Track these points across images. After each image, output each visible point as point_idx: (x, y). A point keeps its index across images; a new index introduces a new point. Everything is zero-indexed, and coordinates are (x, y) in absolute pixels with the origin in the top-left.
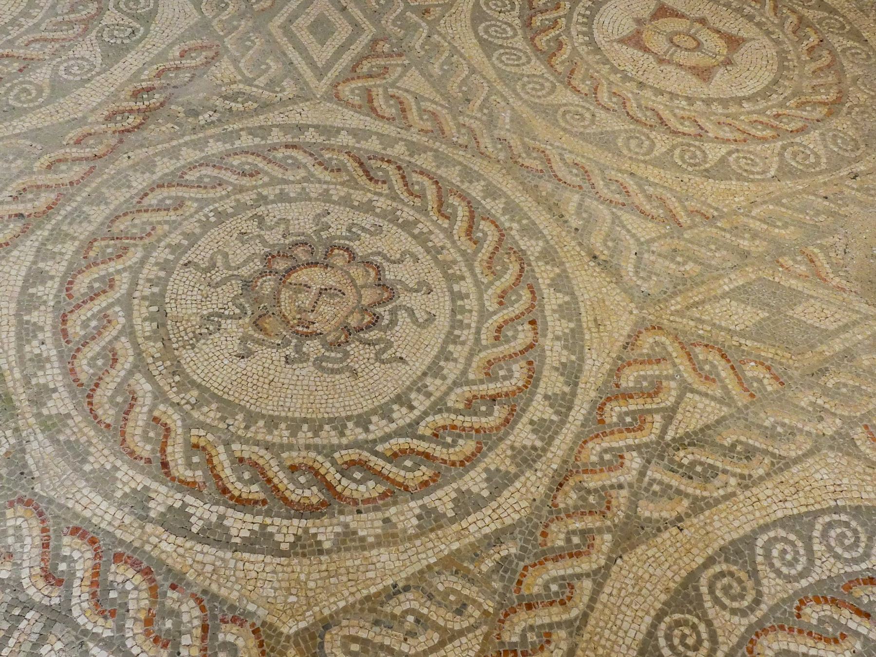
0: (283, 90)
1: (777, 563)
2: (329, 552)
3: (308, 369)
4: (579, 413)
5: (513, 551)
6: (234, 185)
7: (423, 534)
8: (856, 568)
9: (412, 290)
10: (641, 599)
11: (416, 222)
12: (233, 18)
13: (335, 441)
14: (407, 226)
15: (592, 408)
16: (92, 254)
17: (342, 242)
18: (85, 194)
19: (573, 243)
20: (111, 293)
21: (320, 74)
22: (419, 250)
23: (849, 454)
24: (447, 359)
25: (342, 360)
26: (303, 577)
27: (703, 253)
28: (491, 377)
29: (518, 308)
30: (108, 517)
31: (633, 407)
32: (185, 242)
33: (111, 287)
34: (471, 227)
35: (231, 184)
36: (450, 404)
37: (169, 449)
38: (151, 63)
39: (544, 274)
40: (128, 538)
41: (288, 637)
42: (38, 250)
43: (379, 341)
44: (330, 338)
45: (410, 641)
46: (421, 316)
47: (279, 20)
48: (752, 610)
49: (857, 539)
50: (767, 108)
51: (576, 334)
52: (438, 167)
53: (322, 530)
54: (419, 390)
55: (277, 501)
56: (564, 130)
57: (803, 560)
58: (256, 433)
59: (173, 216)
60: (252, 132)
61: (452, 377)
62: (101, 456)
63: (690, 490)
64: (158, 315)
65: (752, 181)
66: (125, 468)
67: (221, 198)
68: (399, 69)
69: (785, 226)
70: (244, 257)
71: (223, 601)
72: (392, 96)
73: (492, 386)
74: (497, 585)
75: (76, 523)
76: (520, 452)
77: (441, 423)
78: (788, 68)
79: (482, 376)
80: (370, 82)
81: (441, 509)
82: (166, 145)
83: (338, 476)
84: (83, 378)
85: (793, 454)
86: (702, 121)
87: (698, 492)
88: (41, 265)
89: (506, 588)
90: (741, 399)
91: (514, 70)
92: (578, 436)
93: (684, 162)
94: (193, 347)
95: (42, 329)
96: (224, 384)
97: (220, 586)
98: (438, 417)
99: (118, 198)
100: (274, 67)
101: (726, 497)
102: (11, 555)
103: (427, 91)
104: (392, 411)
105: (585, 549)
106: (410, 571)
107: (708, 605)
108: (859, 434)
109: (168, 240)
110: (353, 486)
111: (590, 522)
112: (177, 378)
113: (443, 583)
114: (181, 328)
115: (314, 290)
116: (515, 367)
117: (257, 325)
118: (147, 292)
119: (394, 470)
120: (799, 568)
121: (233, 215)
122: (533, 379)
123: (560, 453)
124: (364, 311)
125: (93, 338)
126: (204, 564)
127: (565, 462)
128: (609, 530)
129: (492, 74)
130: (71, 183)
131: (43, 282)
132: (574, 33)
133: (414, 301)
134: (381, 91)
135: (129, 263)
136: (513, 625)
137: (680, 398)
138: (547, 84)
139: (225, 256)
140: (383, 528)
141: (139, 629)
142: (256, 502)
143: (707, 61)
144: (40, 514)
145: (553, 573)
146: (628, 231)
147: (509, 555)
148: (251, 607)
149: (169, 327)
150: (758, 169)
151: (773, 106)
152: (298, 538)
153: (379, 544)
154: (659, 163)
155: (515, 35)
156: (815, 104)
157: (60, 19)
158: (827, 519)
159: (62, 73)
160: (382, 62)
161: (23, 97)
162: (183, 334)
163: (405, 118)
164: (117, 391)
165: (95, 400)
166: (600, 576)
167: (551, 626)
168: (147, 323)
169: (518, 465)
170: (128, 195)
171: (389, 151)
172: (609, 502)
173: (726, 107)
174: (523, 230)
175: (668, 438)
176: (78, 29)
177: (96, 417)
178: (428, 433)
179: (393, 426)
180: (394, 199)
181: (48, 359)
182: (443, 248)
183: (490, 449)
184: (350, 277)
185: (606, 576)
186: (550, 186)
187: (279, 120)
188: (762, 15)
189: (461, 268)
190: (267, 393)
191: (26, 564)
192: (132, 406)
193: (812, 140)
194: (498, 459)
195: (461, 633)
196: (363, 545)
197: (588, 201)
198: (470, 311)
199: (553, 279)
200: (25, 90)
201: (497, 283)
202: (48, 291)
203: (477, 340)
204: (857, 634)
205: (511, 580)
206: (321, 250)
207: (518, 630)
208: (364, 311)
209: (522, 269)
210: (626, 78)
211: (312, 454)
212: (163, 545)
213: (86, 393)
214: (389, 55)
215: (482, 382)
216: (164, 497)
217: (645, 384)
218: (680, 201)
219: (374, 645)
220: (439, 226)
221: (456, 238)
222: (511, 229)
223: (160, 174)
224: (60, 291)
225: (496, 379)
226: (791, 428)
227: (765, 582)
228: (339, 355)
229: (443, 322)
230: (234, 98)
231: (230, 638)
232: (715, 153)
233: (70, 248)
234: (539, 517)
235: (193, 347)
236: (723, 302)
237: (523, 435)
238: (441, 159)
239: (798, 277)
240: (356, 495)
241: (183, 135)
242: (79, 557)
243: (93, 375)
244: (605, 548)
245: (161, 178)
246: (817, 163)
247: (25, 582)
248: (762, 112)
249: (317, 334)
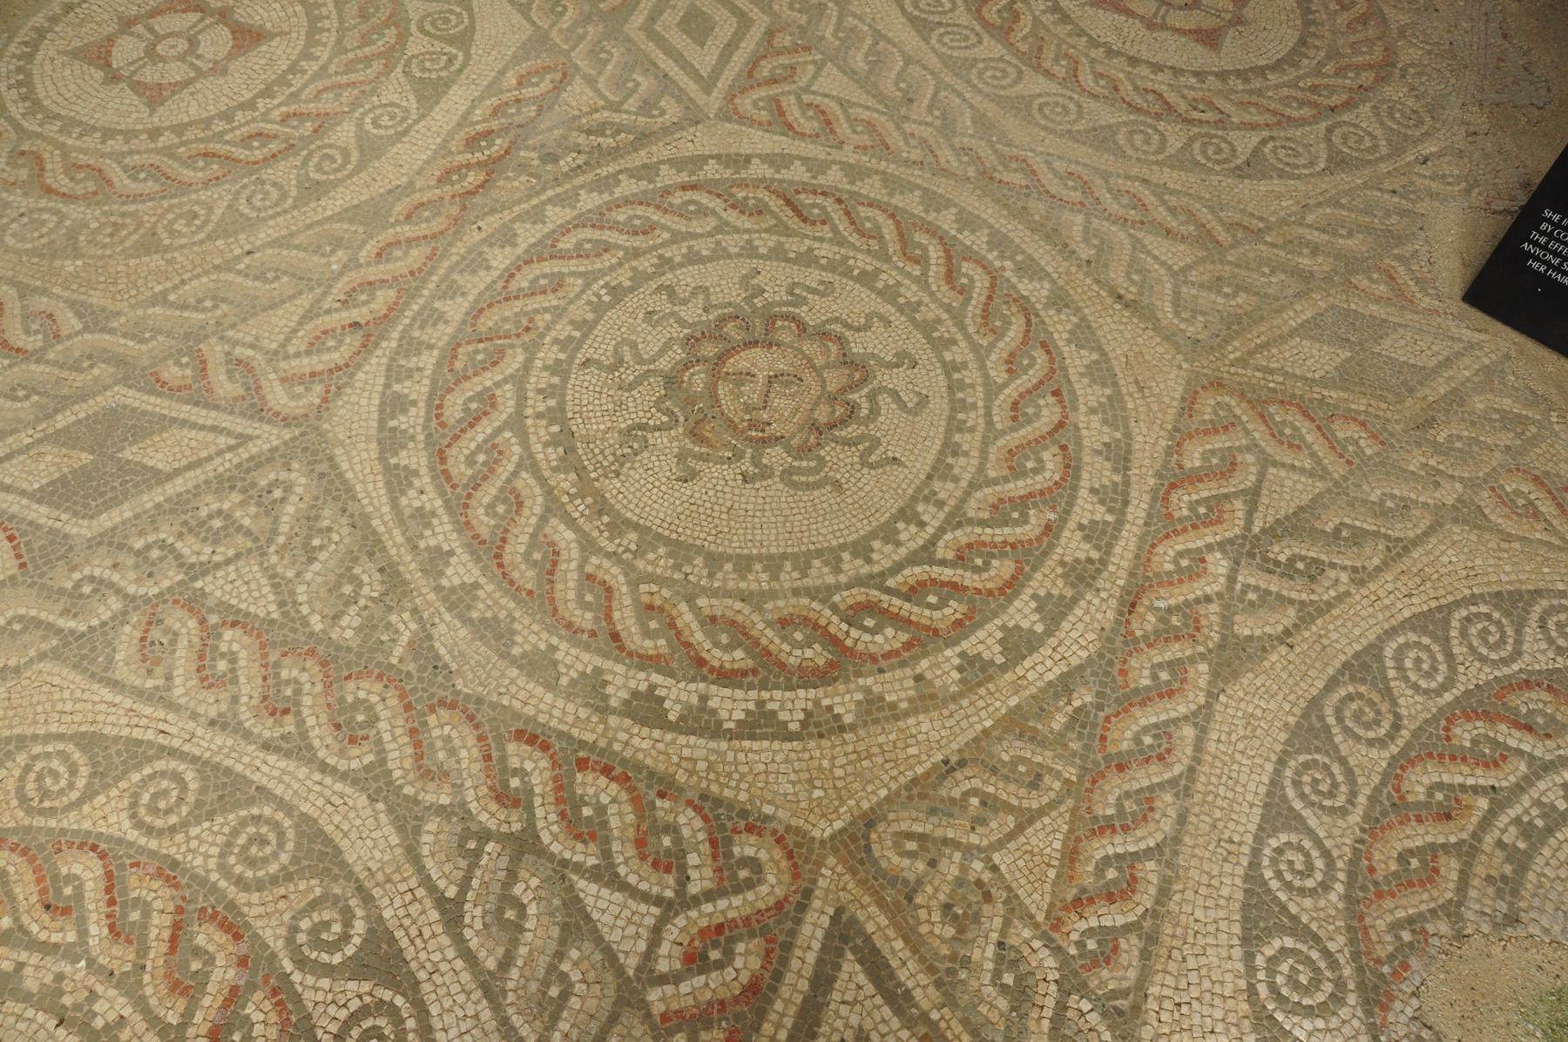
0: (663, 112)
1: (1413, 677)
3: (776, 484)
4: (1137, 511)
5: (1088, 699)
7: (970, 690)
8: (1506, 671)
9: (890, 366)
10: (1256, 743)
11: (878, 271)
12: (576, 24)
13: (830, 579)
14: (866, 278)
15: (1154, 500)
16: (458, 365)
18: (431, 286)
19: (1088, 281)
20: (495, 415)
21: (707, 85)
22: (887, 309)
23: (1479, 527)
24: (955, 454)
25: (817, 470)
26: (826, 763)
28: (1017, 473)
30: (556, 713)
31: (1205, 494)
32: (577, 334)
33: (493, 406)
35: (618, 247)
36: (971, 514)
37: (616, 615)
38: (481, 98)
39: (1059, 326)
40: (589, 737)
41: (823, 842)
42: (389, 369)
44: (796, 442)
45: (979, 829)
46: (910, 399)
47: (638, 19)
48: (1392, 739)
49: (1503, 633)
50: (1300, 78)
52: (891, 195)
53: (838, 699)
54: (926, 500)
55: (767, 669)
56: (1045, 128)
57: (1443, 668)
58: (725, 580)
59: (552, 300)
60: (634, 174)
62: (531, 635)
63: (1294, 595)
65: (1299, 177)
66: (564, 646)
67: (612, 268)
68: (811, 68)
69: (1350, 234)
70: (659, 344)
72: (810, 105)
73: (1020, 483)
74: (1075, 746)
75: (520, 725)
77: (964, 540)
78: (1314, 23)
79: (1006, 472)
80: (776, 90)
81: (986, 655)
82: (525, 206)
83: (844, 626)
84: (484, 532)
85: (1411, 534)
87: (1304, 596)
88: (396, 387)
89: (1086, 747)
90: (1338, 470)
93: (1208, 158)
95: (416, 473)
97: (722, 786)
98: (958, 533)
101: (1340, 598)
102: (447, 774)
103: (856, 95)
104: (897, 532)
105: (1176, 685)
106: (962, 740)
107: (1338, 739)
108: (1485, 498)
109: (553, 334)
110: (867, 637)
111: (1175, 651)
112: (606, 519)
115: (761, 377)
116: (1046, 456)
117: (695, 435)
118: (541, 407)
119: (916, 609)
120: (1440, 679)
121: (632, 289)
122: (1072, 469)
123: (1125, 564)
124: (832, 399)
125: (485, 478)
127: (1132, 574)
128: (1203, 657)
129: (936, 64)
130: (412, 273)
131: (404, 411)
133: (894, 379)
134: (792, 99)
135: (509, 371)
136: (1104, 793)
137: (1262, 475)
138: (1010, 70)
139: (633, 345)
140: (916, 689)
141: (631, 851)
142: (744, 673)
143: (1209, 23)
144: (471, 718)
145: (1144, 722)
146: (1156, 258)
148: (768, 810)
151: (1306, 76)
152: (808, 714)
153: (914, 711)
156: (1360, 68)
157: (351, 55)
158: (1464, 613)
159: (369, 127)
160: (784, 60)
161: (326, 166)
163: (833, 132)
165: (507, 559)
166: (1202, 718)
167: (1151, 788)
169: (1073, 585)
170: (489, 280)
171: (821, 180)
172: (1197, 621)
173: (1247, 81)
174: (1019, 269)
175: (1256, 529)
176: (377, 66)
177: (512, 583)
178: (950, 555)
179: (903, 551)
182: (919, 303)
183: (1034, 569)
185: (1209, 717)
186: (1042, 207)
187: (666, 154)
189: (948, 328)
191: (468, 784)
192: (555, 563)
195: (1041, 812)
197: (1096, 223)
198: (972, 386)
199: (1071, 332)
201: (1001, 344)
202: (412, 420)
203: (990, 424)
204: (1519, 752)
205: (1091, 736)
207: (1112, 799)
208: (832, 399)
210: (1110, 53)
211: (805, 601)
212: (636, 741)
213: (490, 551)
214: (794, 50)
215: (1006, 480)
216: (622, 682)
217: (1215, 461)
218: (1212, 210)
219: (934, 840)
220: (909, 275)
222: (1003, 268)
223: (524, 246)
224: (428, 420)
225: (1023, 474)
226: (1402, 499)
227: (1402, 701)
229: (939, 404)
230: (600, 130)
231: (750, 852)
232: (1245, 143)
233: (428, 360)
234: (1113, 651)
236: (1293, 343)
237: (1072, 546)
239: (1378, 300)
241: (544, 190)
242: (536, 770)
243: (497, 526)
244: (1202, 683)
245: (527, 251)
246: (1375, 147)
248: (1293, 84)
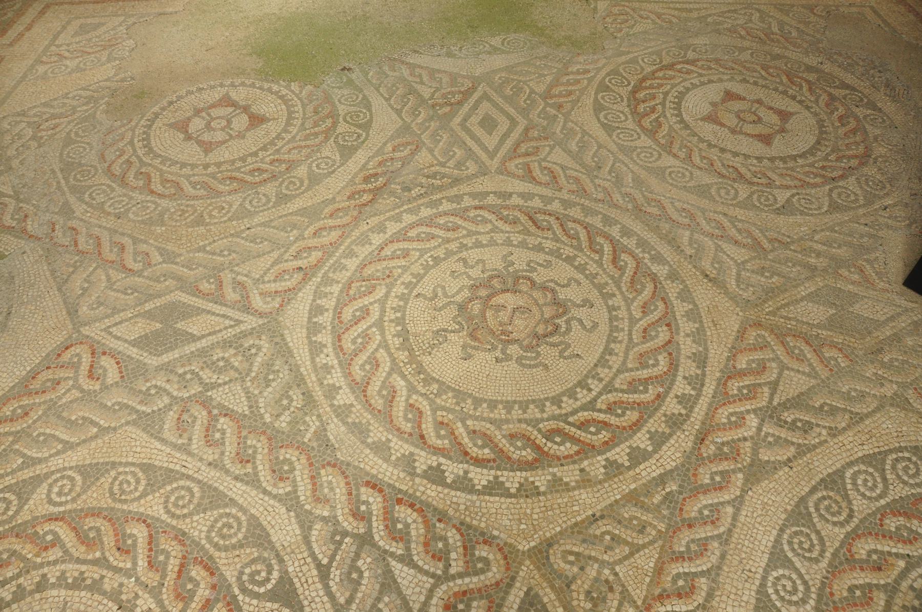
0: (467, 169)
1: (862, 489)
2: (544, 494)
3: (513, 364)
4: (709, 389)
5: (674, 488)
7: (610, 479)
9: (579, 306)
10: (768, 519)
11: (576, 256)
12: (425, 120)
13: (539, 416)
14: (569, 260)
15: (718, 384)
16: (351, 292)
21: (492, 155)
22: (580, 277)
24: (610, 354)
27: (785, 269)
28: (644, 366)
29: (656, 315)
30: (388, 474)
31: (747, 383)
33: (368, 314)
34: (614, 258)
36: (617, 386)
37: (424, 426)
38: (373, 157)
39: (672, 290)
40: (404, 488)
41: (523, 552)
42: (315, 292)
43: (561, 343)
44: (525, 343)
45: (609, 553)
46: (588, 324)
47: (457, 120)
48: (848, 522)
51: (701, 331)
52: (586, 217)
54: (593, 377)
55: (501, 460)
57: (880, 486)
58: (482, 412)
59: (403, 262)
60: (449, 199)
61: (616, 366)
62: (378, 433)
63: (795, 440)
66: (395, 440)
67: (435, 247)
69: (839, 247)
71: (476, 530)
73: (645, 371)
75: (368, 479)
76: (671, 418)
77: (612, 400)
79: (637, 365)
80: (528, 159)
83: (544, 440)
85: (865, 411)
86: (770, 174)
88: (319, 302)
90: (824, 373)
91: (629, 144)
92: (710, 405)
95: (325, 346)
97: (472, 518)
98: (609, 395)
99: (363, 252)
100: (459, 153)
101: (821, 443)
102: (328, 501)
103: (570, 163)
106: (603, 504)
107: (816, 520)
108: (910, 394)
110: (556, 447)
111: (725, 466)
112: (422, 376)
113: (628, 512)
115: (510, 308)
116: (660, 358)
117: (472, 336)
118: (393, 317)
120: (878, 491)
121: (444, 259)
122: (674, 366)
123: (699, 418)
124: (547, 322)
125: (361, 351)
126: (459, 505)
127: (703, 423)
128: (740, 470)
129: (614, 148)
132: (668, 115)
133: (582, 313)
134: (536, 164)
136: (679, 539)
137: (780, 374)
139: (443, 288)
142: (489, 461)
143: (766, 131)
144: (343, 473)
145: (704, 502)
147: (672, 491)
148: (496, 533)
150: (814, 206)
152: (521, 485)
153: (579, 487)
154: (743, 205)
155: (627, 119)
156: (850, 158)
158: (894, 456)
159: (315, 168)
164: (383, 387)
165: (369, 393)
166: (738, 503)
167: (706, 538)
169: (670, 427)
171: (549, 207)
173: (785, 162)
175: (775, 403)
176: (321, 138)
177: (370, 405)
178: (604, 407)
179: (579, 403)
180: (557, 241)
181: (332, 367)
182: (597, 274)
183: (650, 417)
185: (742, 503)
186: (667, 226)
187: (467, 190)
188: (802, 95)
189: (611, 288)
191: (339, 506)
192: (394, 397)
193: (851, 183)
194: (655, 424)
195: (644, 546)
196: (568, 488)
197: (696, 236)
200: (291, 182)
202: (325, 319)
206: (510, 281)
207: (684, 543)
208: (547, 322)
209: (656, 287)
210: (710, 145)
211: (524, 426)
213: (361, 388)
215: (637, 369)
216: (424, 459)
218: (761, 231)
219: (584, 557)
220: (592, 259)
224: (334, 319)
225: (647, 367)
227: (854, 502)
229: (604, 328)
230: (434, 176)
231: (484, 554)
232: (782, 196)
233: (336, 289)
234: (690, 463)
237: (672, 406)
238: (586, 210)
239: (853, 283)
240: (558, 453)
242: (374, 502)
244: (739, 484)
246: (857, 200)
247: (340, 518)
248: (812, 165)
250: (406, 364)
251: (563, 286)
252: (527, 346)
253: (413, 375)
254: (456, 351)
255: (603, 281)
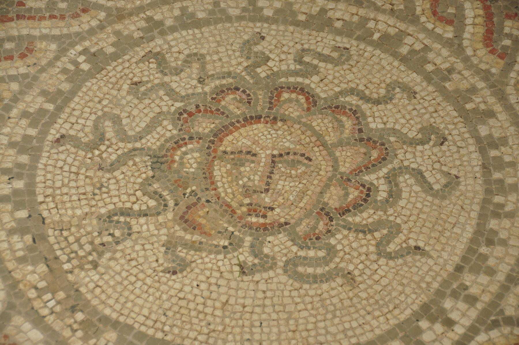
3: (278, 277)
6: (107, 9)
9: (413, 143)
11: (402, 34)
14: (388, 43)
17: (292, 79)
22: (412, 78)
24: (490, 242)
25: (326, 261)
32: (51, 107)
44: (302, 229)
46: (437, 181)
54: (455, 295)
64: (29, 224)
67: (92, 32)
70: (147, 120)
94: (95, 265)
96: (154, 317)
109: (21, 106)
112: (80, 316)
114: (71, 239)
115: (264, 156)
117: (186, 221)
121: (115, 57)
124: (345, 180)
133: (421, 158)
139: (117, 120)
149: (52, 240)
162: (75, 247)
168: (16, 238)
182: (450, 70)
184: (315, 133)
189: (484, 98)
190: (222, 323)
206: (261, 97)
208: (345, 180)
220: (439, 38)
221: (469, 52)
228: (321, 254)
229: (472, 187)
235: (95, 265)
249: (281, 225)
250: (41, 292)
251: (377, 102)
252: (307, 236)
253: (60, 316)
254: (155, 255)
255: (464, 85)
